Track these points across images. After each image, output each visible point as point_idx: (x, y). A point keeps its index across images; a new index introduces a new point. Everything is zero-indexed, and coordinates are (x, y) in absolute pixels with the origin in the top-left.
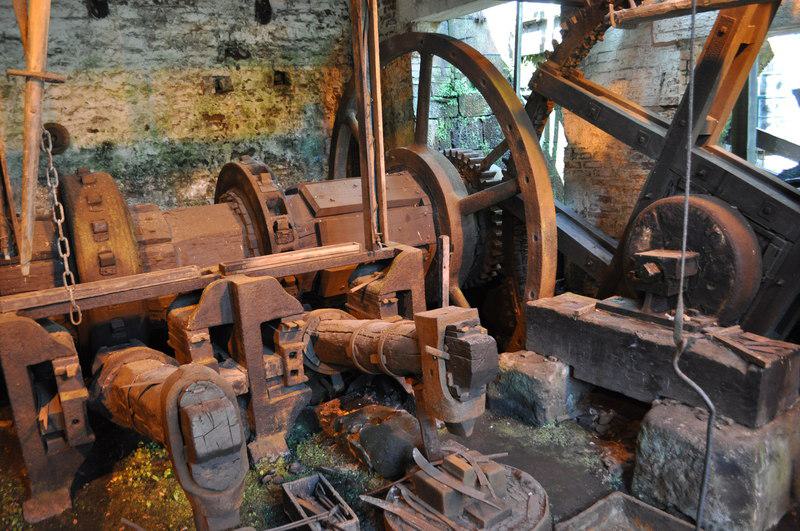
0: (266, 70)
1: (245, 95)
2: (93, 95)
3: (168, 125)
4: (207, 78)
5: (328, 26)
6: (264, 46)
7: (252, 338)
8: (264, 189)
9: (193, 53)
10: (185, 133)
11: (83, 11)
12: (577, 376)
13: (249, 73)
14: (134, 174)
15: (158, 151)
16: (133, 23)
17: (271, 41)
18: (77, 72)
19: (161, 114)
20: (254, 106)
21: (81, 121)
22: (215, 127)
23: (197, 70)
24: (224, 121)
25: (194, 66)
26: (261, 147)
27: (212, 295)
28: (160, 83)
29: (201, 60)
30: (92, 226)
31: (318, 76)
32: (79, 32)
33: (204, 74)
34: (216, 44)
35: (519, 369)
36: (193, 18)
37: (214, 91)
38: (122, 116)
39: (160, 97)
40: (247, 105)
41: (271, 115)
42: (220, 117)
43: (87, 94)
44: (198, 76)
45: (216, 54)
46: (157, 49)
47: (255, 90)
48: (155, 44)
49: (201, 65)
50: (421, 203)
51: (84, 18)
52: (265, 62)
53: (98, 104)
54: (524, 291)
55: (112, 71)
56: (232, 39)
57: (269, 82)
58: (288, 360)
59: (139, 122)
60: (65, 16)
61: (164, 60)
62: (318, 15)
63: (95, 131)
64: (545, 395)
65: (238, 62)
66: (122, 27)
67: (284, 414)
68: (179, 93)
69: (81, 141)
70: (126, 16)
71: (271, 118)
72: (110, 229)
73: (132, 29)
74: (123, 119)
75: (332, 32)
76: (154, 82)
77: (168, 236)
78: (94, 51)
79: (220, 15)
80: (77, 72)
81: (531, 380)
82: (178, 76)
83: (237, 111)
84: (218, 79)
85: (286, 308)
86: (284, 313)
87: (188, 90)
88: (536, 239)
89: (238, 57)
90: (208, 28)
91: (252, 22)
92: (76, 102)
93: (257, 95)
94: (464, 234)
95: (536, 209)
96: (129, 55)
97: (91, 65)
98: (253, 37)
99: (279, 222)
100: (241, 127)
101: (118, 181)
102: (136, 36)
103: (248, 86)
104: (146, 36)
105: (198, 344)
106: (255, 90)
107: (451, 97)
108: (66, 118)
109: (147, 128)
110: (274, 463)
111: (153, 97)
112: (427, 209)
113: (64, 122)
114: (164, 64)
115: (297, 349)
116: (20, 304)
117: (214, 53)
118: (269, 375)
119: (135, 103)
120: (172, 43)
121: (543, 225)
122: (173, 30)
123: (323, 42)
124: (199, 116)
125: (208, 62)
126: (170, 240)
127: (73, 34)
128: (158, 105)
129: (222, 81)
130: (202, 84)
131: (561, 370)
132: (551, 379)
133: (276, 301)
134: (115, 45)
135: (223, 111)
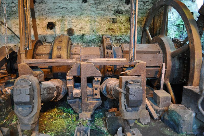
0: (127, 17)
1: (120, 24)
2: (81, 22)
3: (99, 31)
4: (110, 19)
5: (147, 5)
6: (127, 10)
7: (84, 81)
8: (107, 43)
9: (107, 12)
10: (103, 33)
11: (81, 1)
12: (198, 117)
13: (122, 18)
14: (89, 42)
15: (96, 37)
16: (93, 4)
17: (129, 9)
18: (78, 16)
19: (97, 28)
20: (123, 27)
21: (78, 28)
22: (111, 32)
23: (108, 17)
24: (114, 31)
25: (107, 15)
26: (123, 38)
27: (74, 68)
28: (98, 20)
29: (109, 14)
30: (57, 47)
31: (142, 19)
32: (80, 6)
33: (110, 18)
34: (114, 10)
35: (175, 110)
36: (108, 3)
37: (112, 22)
38: (88, 28)
39: (97, 23)
40: (121, 26)
41: (127, 30)
42: (113, 29)
43: (80, 22)
44: (108, 18)
45: (113, 12)
46: (98, 11)
47: (123, 23)
48: (98, 10)
49: (109, 15)
50: (159, 53)
51: (81, 3)
52: (127, 15)
53: (82, 24)
54: (187, 83)
55: (87, 16)
56: (118, 8)
57: (128, 20)
58: (94, 90)
59: (92, 29)
60: (77, 2)
61: (100, 14)
62: (144, 2)
63: (81, 31)
64: (182, 122)
65: (119, 15)
66: (90, 5)
67: (92, 107)
68: (103, 22)
69: (77, 33)
70: (91, 2)
71: (127, 30)
72: (62, 48)
73: (92, 6)
74: (88, 28)
75: (148, 7)
76: (97, 19)
77: (79, 53)
78: (83, 11)
79: (115, 2)
80: (78, 16)
81: (179, 115)
82: (103, 18)
83: (118, 28)
84: (114, 19)
85: (96, 74)
86: (94, 75)
87: (105, 22)
88: (193, 64)
89: (119, 13)
90: (112, 5)
91: (124, 4)
92: (77, 23)
93: (124, 24)
94: (172, 64)
95: (194, 53)
96: (91, 12)
97: (82, 15)
98: (124, 8)
99: (108, 52)
100: (118, 32)
101: (85, 44)
102: (93, 7)
103: (121, 21)
104: (96, 8)
105: (70, 80)
106: (123, 23)
107: (181, 25)
108: (74, 27)
109: (93, 31)
110: (85, 121)
111: (96, 23)
112: (161, 55)
113: (74, 28)
114: (100, 15)
115: (97, 87)
116: (28, 61)
117: (113, 12)
118: (88, 94)
119: (91, 24)
120: (102, 9)
121: (196, 60)
122: (103, 6)
123: (144, 10)
124: (107, 29)
125: (111, 14)
126: (79, 54)
127: (78, 7)
128: (97, 25)
129: (115, 20)
130: (109, 20)
131: (191, 114)
132: (186, 116)
133: (92, 71)
134: (88, 10)
135: (114, 28)
